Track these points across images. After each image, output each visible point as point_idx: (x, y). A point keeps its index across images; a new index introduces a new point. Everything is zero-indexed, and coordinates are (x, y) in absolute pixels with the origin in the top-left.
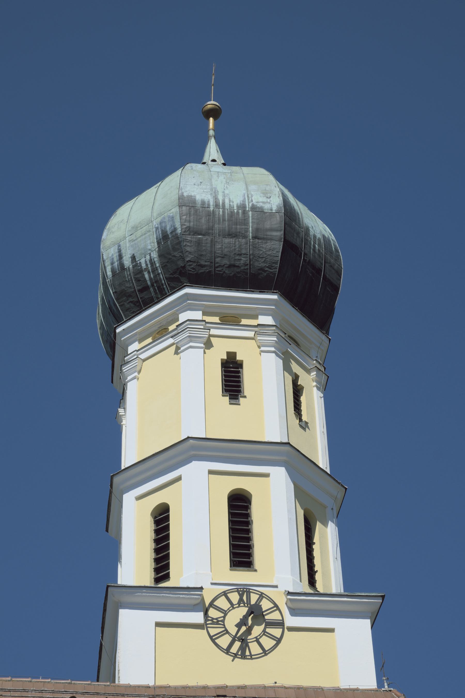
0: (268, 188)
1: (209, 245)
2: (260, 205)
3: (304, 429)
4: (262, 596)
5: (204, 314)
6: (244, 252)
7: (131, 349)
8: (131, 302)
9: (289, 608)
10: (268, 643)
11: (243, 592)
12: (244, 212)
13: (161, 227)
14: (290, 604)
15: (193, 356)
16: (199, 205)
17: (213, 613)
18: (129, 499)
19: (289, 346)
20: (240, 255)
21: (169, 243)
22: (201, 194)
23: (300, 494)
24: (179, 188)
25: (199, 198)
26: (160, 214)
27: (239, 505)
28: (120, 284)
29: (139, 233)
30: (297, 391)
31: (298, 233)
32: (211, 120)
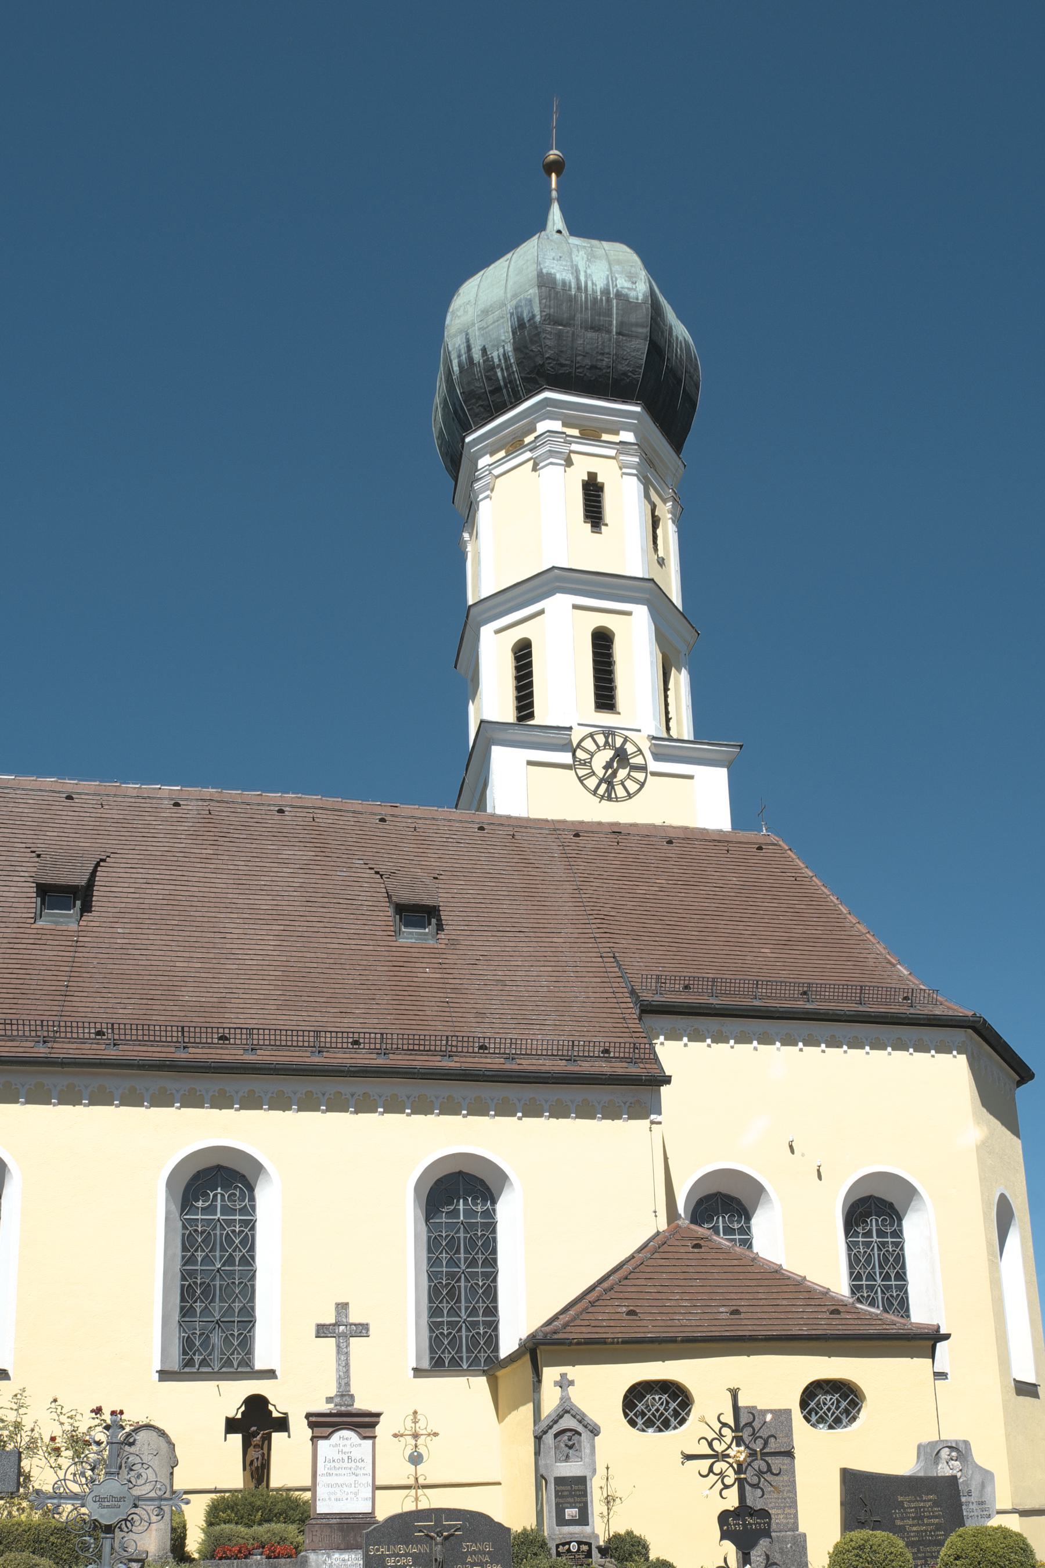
0: (633, 270)
1: (570, 339)
2: (625, 291)
3: (661, 566)
4: (626, 739)
5: (564, 425)
6: (607, 350)
7: (483, 462)
8: (481, 406)
9: (652, 753)
10: (632, 787)
11: (609, 734)
12: (609, 300)
13: (517, 313)
14: (654, 750)
15: (552, 472)
16: (559, 287)
17: (580, 754)
18: (487, 632)
19: (650, 472)
20: (603, 354)
21: (525, 332)
22: (562, 274)
23: (661, 638)
24: (538, 263)
25: (558, 276)
26: (515, 296)
27: (602, 643)
28: (469, 383)
29: (490, 319)
30: (655, 522)
31: (662, 332)
32: (553, 175)
